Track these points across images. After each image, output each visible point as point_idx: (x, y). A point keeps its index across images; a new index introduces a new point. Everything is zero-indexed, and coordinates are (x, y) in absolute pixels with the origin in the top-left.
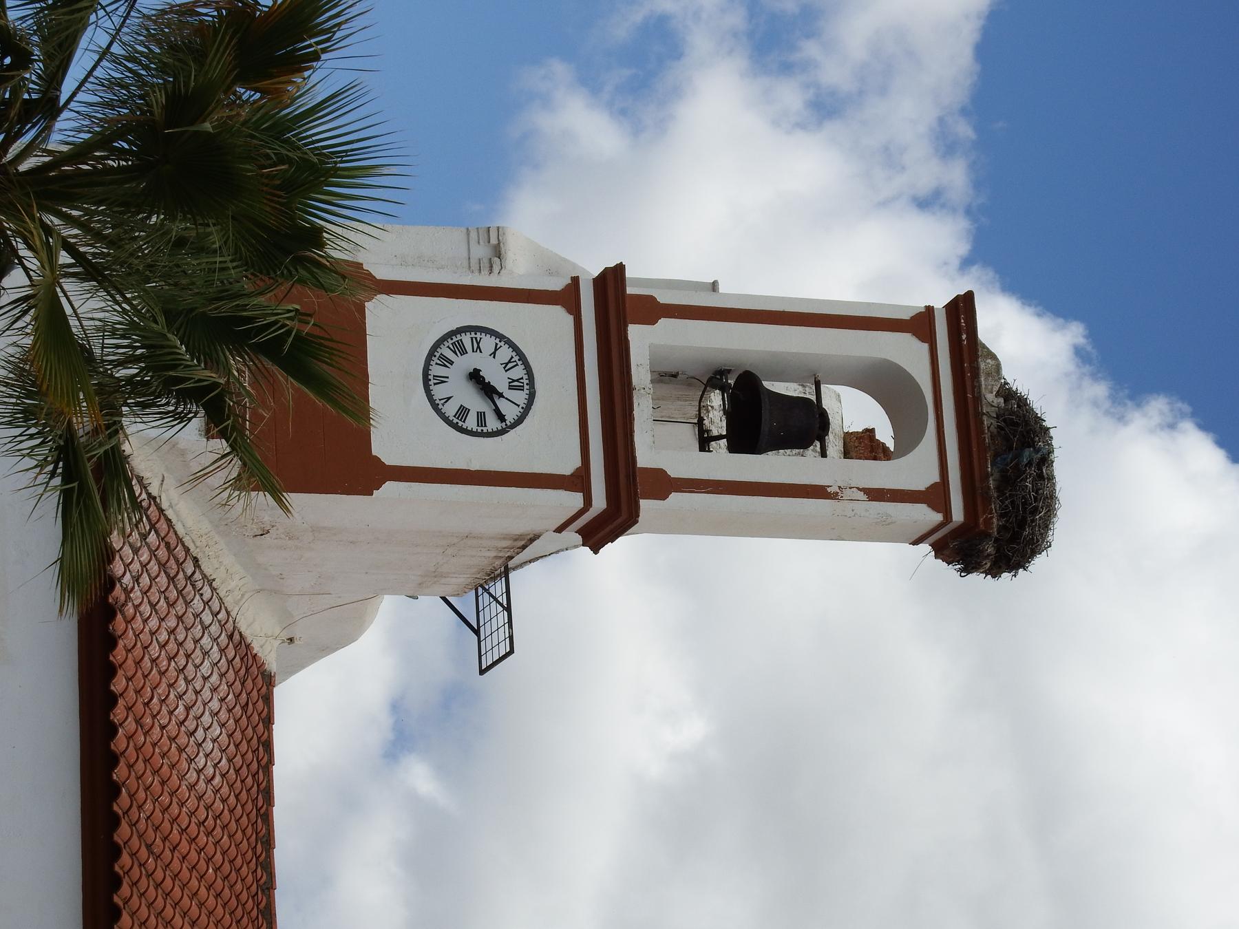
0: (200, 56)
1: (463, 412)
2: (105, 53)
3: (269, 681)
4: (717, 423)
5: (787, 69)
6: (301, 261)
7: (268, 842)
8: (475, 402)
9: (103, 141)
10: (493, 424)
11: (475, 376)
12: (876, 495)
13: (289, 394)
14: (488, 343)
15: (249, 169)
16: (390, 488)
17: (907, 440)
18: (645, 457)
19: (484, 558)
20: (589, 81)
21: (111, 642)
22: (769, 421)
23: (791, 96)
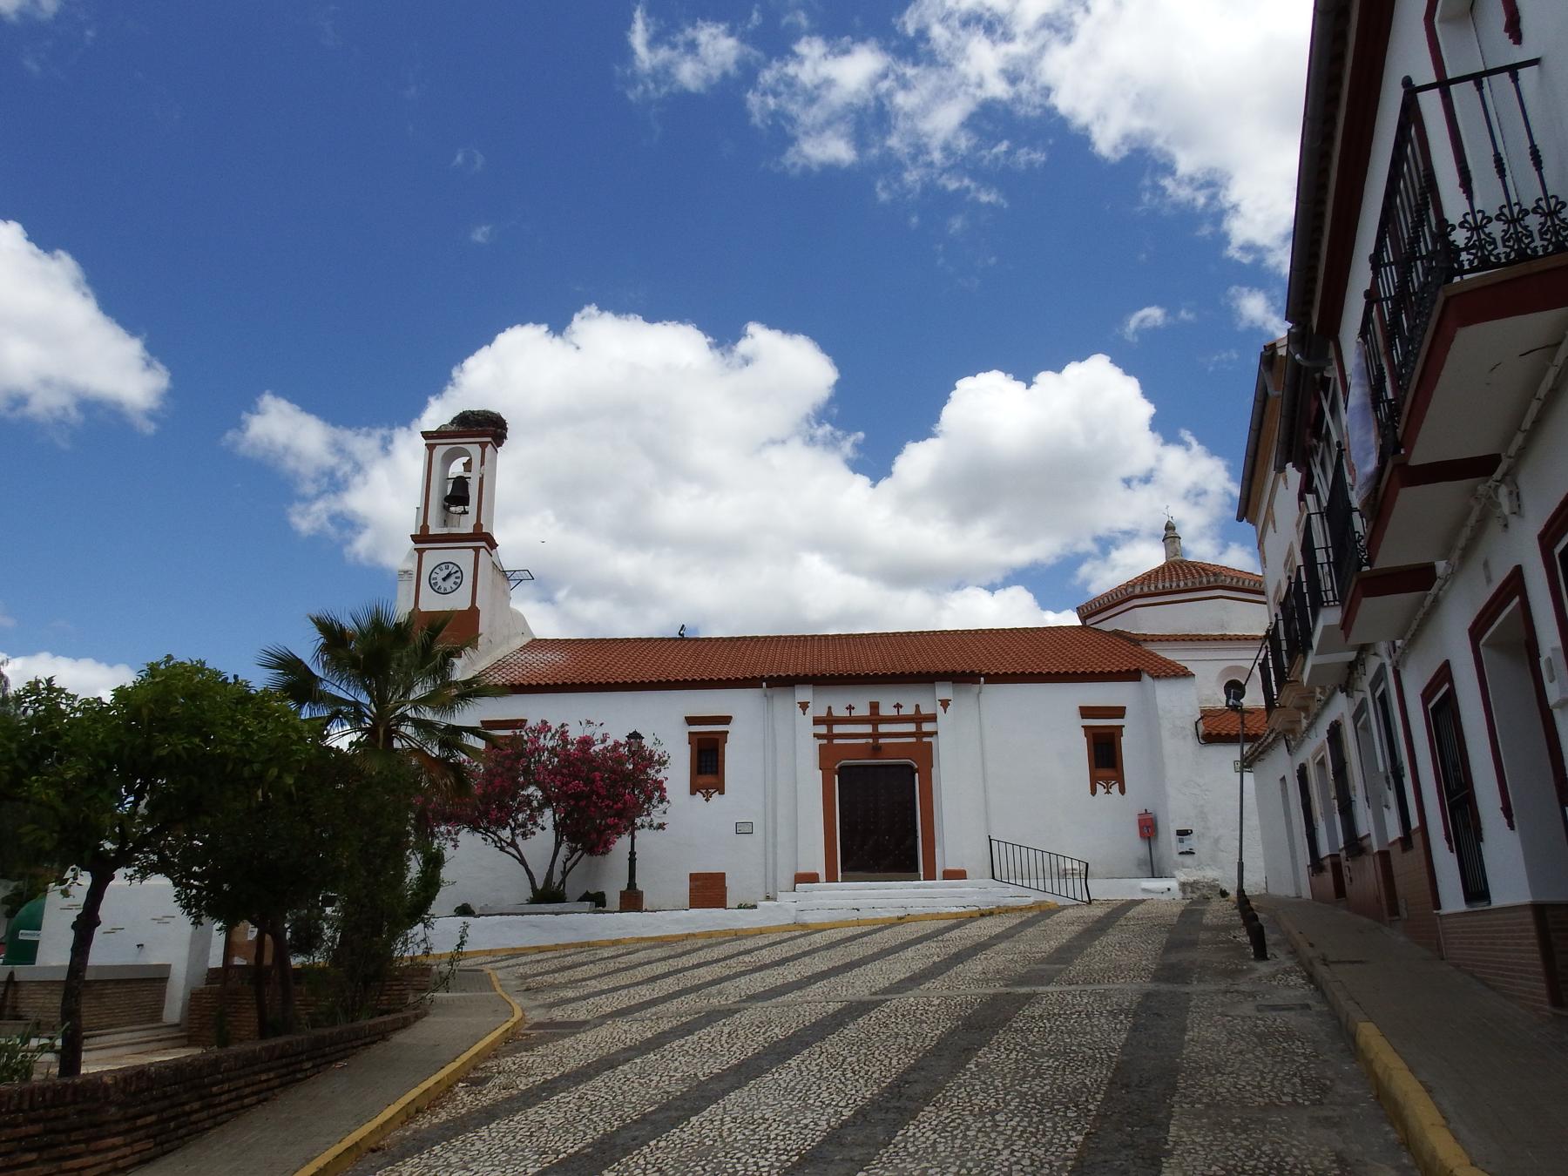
1: (455, 583)
3: (534, 640)
4: (460, 509)
5: (346, 481)
8: (452, 579)
10: (459, 574)
11: (444, 579)
12: (482, 463)
14: (434, 575)
17: (466, 453)
18: (470, 530)
19: (499, 577)
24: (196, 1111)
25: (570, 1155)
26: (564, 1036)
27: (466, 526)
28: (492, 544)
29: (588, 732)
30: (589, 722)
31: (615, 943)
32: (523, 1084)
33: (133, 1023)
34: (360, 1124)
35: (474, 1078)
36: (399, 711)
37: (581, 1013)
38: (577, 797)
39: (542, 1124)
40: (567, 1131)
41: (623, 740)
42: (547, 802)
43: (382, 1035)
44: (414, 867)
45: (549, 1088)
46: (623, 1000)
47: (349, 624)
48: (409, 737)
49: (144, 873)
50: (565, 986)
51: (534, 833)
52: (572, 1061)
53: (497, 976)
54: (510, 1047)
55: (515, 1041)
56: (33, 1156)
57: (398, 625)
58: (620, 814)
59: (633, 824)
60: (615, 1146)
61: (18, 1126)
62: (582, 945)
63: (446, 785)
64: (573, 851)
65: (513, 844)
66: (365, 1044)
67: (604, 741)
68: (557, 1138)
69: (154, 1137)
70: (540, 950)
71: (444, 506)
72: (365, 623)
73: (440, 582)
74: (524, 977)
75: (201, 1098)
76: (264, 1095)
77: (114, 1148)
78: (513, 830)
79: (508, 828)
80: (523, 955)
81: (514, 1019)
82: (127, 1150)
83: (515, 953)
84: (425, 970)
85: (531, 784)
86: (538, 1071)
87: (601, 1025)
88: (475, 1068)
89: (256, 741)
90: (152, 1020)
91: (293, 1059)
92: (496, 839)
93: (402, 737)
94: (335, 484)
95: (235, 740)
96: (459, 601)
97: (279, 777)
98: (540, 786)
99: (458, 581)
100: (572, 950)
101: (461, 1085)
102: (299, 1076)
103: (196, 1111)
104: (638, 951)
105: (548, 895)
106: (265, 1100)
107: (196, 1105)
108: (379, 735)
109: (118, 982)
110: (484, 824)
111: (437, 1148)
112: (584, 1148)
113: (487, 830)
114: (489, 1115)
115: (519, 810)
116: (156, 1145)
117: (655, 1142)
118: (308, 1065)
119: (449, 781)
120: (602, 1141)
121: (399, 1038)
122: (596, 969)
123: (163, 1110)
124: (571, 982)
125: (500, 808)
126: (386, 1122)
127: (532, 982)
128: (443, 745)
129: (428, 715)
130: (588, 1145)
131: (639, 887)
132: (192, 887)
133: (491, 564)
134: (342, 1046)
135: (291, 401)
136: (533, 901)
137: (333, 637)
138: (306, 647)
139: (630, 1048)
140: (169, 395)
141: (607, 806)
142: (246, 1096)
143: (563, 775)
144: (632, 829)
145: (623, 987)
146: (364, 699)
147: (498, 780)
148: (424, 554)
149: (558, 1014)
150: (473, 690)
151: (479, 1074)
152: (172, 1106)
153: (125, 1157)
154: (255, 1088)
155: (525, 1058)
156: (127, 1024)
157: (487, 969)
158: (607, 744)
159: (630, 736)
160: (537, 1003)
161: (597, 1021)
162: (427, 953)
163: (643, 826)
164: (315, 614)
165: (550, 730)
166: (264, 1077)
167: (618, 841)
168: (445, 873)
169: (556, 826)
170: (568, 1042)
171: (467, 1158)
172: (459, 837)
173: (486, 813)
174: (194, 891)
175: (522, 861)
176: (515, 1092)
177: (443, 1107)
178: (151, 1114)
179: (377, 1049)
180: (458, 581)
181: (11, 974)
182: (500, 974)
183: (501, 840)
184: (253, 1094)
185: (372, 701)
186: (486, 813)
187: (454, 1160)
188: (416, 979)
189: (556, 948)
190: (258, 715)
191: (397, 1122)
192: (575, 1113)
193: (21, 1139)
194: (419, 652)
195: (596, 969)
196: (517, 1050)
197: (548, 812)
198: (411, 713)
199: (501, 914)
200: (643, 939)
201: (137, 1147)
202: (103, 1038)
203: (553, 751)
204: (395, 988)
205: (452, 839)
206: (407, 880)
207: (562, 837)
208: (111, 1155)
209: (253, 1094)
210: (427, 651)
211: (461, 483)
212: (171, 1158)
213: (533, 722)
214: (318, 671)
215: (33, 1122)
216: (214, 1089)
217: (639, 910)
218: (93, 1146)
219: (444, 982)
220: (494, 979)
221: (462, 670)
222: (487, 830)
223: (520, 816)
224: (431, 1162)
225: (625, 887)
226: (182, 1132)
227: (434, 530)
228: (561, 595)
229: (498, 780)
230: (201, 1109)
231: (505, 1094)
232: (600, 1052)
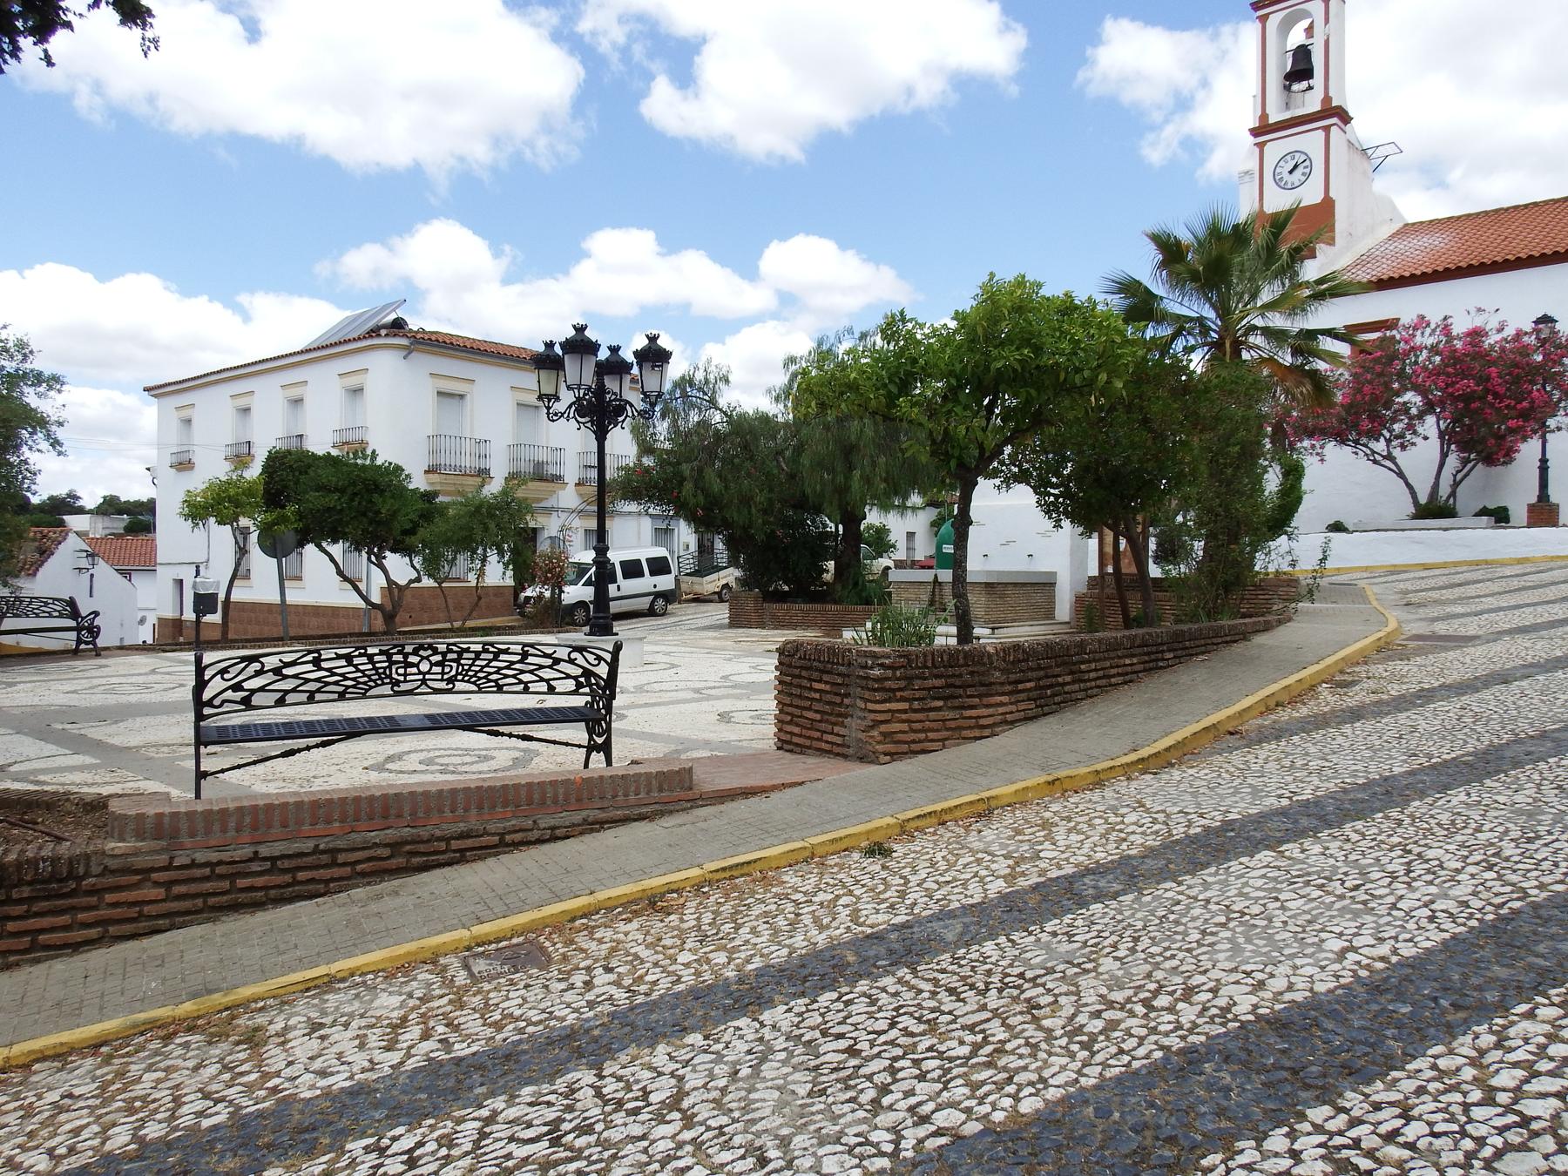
0: (1178, 274)
1: (1304, 174)
2: (1181, 303)
3: (1407, 225)
4: (1304, 84)
5: (1193, 98)
6: (1244, 230)
7: (1469, 215)
8: (1300, 170)
9: (1209, 300)
10: (1307, 163)
11: (1291, 172)
12: (1327, 21)
13: (1294, 227)
14: (1278, 170)
15: (1214, 253)
16: (1331, 195)
17: (1306, 14)
18: (1317, 107)
19: (1357, 157)
20: (1202, 162)
21: (1391, 278)
22: (1301, 67)
23: (1200, 95)
24: (1068, 684)
25: (1446, 761)
26: (1446, 649)
27: (1312, 104)
28: (1345, 118)
29: (1478, 322)
30: (1479, 310)
31: (1521, 561)
32: (1395, 690)
33: (1032, 619)
34: (1217, 708)
35: (1340, 682)
36: (1243, 323)
37: (1471, 627)
38: (1468, 398)
39: (1414, 729)
40: (1444, 738)
41: (1528, 327)
42: (1429, 407)
43: (1243, 636)
44: (1272, 481)
45: (1425, 696)
46: (1527, 617)
47: (1185, 237)
48: (1259, 348)
49: (1007, 482)
50: (1454, 602)
51: (1413, 444)
52: (1455, 673)
53: (1372, 591)
54: (1383, 655)
55: (1386, 650)
56: (940, 703)
57: (1236, 227)
58: (1525, 415)
59: (1544, 425)
60: (1503, 758)
61: (925, 679)
62: (1478, 563)
63: (1302, 393)
64: (1465, 462)
65: (1390, 457)
66: (1227, 642)
67: (1500, 330)
68: (1431, 743)
69: (1035, 700)
70: (1426, 567)
71: (1285, 87)
72: (1201, 232)
74: (1406, 592)
75: (1072, 673)
76: (1130, 678)
77: (1002, 704)
78: (1388, 441)
79: (1382, 439)
80: (1405, 572)
81: (1388, 629)
82: (1013, 708)
83: (1394, 570)
84: (1292, 582)
85: (1408, 390)
86: (1413, 679)
87: (1495, 641)
88: (1342, 672)
89: (1082, 349)
90: (1048, 618)
91: (1154, 649)
92: (1369, 452)
93: (1251, 348)
94: (1183, 103)
95: (1064, 349)
96: (1311, 195)
97: (1108, 382)
98: (1417, 389)
99: (1308, 170)
100: (1465, 568)
101: (1324, 685)
102: (1161, 664)
103: (1068, 684)
104: (1552, 569)
105: (1434, 510)
106: (1131, 681)
107: (1068, 679)
108: (1226, 347)
109: (1015, 584)
110: (1352, 437)
111: (1296, 739)
112: (1463, 755)
113: (1356, 442)
114: (1356, 714)
115: (1394, 420)
116: (1037, 707)
117: (1556, 759)
118: (1169, 655)
119: (1307, 388)
120: (1486, 752)
121: (1260, 639)
122: (1495, 587)
123: (1039, 679)
124: (1461, 599)
125: (1372, 419)
126: (1244, 710)
127: (1414, 598)
128: (1296, 352)
129: (1277, 321)
130: (1468, 754)
131: (1554, 498)
132: (1050, 494)
133: (1346, 143)
134: (1203, 642)
135: (1133, 19)
136: (1415, 517)
137: (1170, 251)
138: (1144, 266)
139: (1531, 665)
140: (1026, 55)
141: (1507, 407)
142: (1113, 676)
143: (1448, 375)
144: (1543, 430)
145: (1528, 605)
146: (1209, 313)
147: (1367, 388)
149: (1441, 628)
150: (1330, 289)
151: (1346, 677)
152: (1047, 677)
153: (1012, 713)
154: (1120, 670)
155: (1399, 666)
156: (1027, 620)
157: (1362, 584)
158: (1505, 334)
159: (1537, 322)
160: (1418, 616)
161: (1492, 637)
162: (1293, 564)
163: (1559, 429)
164: (1153, 226)
165: (1428, 325)
166: (1128, 661)
167: (1523, 447)
168: (1306, 484)
169: (1441, 435)
170: (1451, 655)
171: (1326, 750)
172: (1325, 451)
173: (1355, 426)
174: (1052, 499)
175: (1401, 474)
176: (1385, 697)
177: (1304, 704)
178: (1029, 681)
179: (1238, 648)
181: (936, 576)
182: (1376, 589)
183: (1374, 452)
184: (1119, 675)
185: (1218, 316)
186: (1355, 426)
187: (1312, 750)
189: (1444, 565)
190: (1086, 324)
191: (1256, 712)
192: (1454, 722)
193: (929, 689)
194: (1264, 255)
195: (1495, 587)
196: (1390, 658)
197: (1431, 420)
198: (1259, 322)
199: (1377, 530)
200: (1558, 557)
201: (1022, 706)
203: (1434, 350)
205: (1318, 454)
206: (1266, 493)
207: (1449, 448)
208: (1001, 710)
209: (1119, 675)
210: (1271, 250)
211: (1303, 53)
212: (1051, 719)
213: (1407, 318)
214: (1158, 289)
215: (937, 677)
216: (1083, 667)
217: (1555, 524)
218: (986, 700)
219: (1310, 594)
220: (1369, 593)
221: (1311, 271)
222: (1356, 442)
223: (1396, 426)
224: (1288, 750)
225: (1534, 500)
226: (1057, 699)
227: (1274, 117)
228: (1455, 176)
229: (1367, 388)
230: (1073, 682)
231: (1374, 697)
232: (1492, 666)
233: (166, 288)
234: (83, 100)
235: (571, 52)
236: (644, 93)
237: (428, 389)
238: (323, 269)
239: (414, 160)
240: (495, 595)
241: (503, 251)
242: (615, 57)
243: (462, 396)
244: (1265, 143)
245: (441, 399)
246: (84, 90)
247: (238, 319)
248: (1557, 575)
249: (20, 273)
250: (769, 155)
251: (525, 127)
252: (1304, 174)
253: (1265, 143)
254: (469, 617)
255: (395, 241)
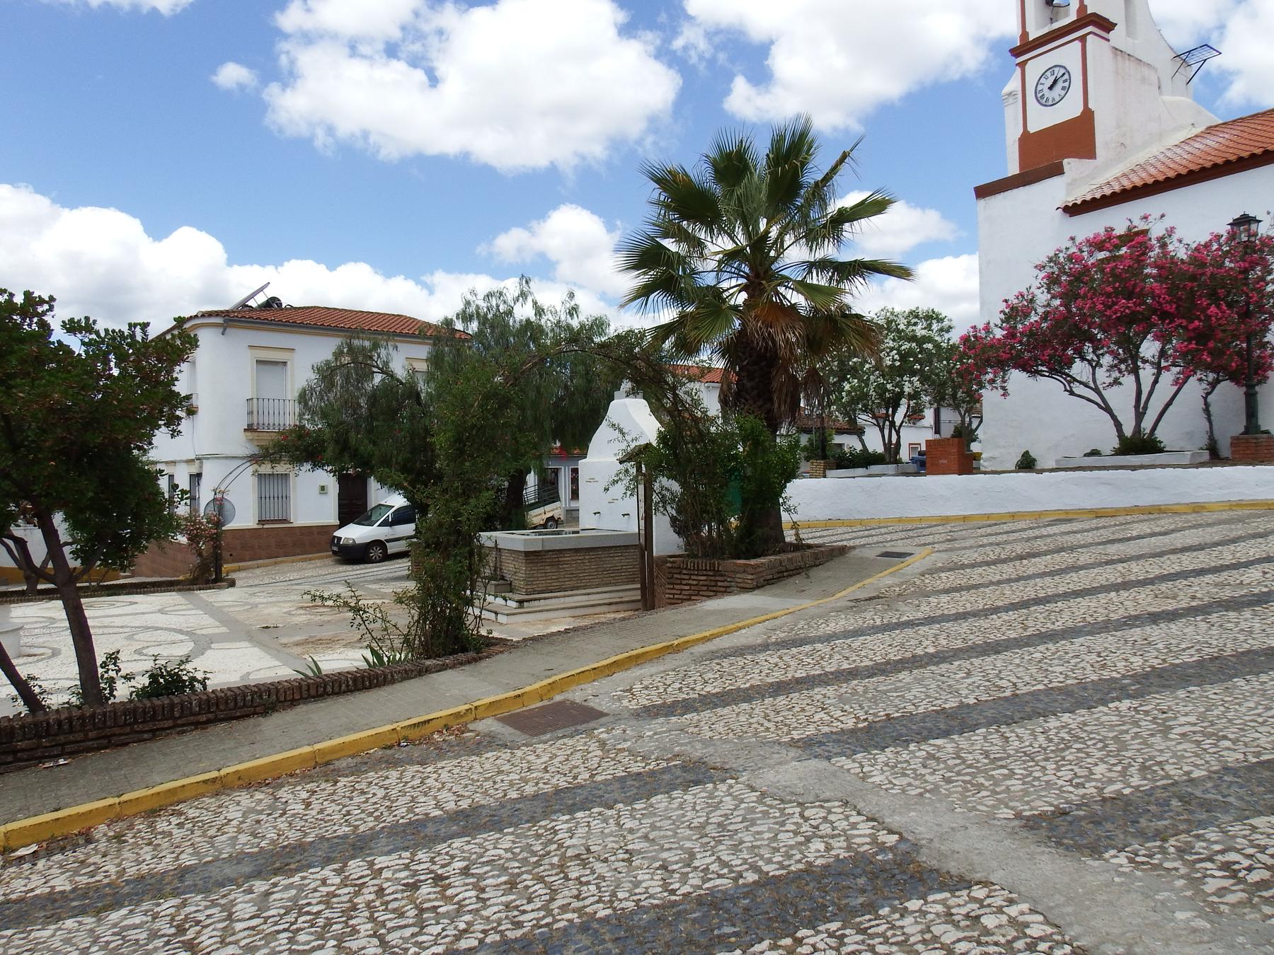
1: (1063, 88)
8: (1060, 84)
10: (1066, 77)
11: (1051, 88)
16: (1090, 106)
73: (1047, 93)
80: (1070, 521)
109: (577, 551)
148: (1027, 67)
175: (1107, 409)
180: (1066, 84)
188: (738, 575)
202: (548, 602)
204: (719, 584)
233: (376, 273)
234: (321, 139)
235: (670, 66)
236: (728, 92)
237: (246, 361)
238: (481, 249)
239: (552, 163)
240: (319, 533)
241: (616, 225)
242: (702, 67)
243: (285, 363)
244: (1026, 62)
245: (261, 367)
246: (320, 133)
247: (425, 292)
248: (1261, 525)
249: (276, 268)
250: (835, 129)
251: (635, 129)
252: (1063, 88)
253: (1026, 62)
254: (103, 579)
255: (534, 224)
